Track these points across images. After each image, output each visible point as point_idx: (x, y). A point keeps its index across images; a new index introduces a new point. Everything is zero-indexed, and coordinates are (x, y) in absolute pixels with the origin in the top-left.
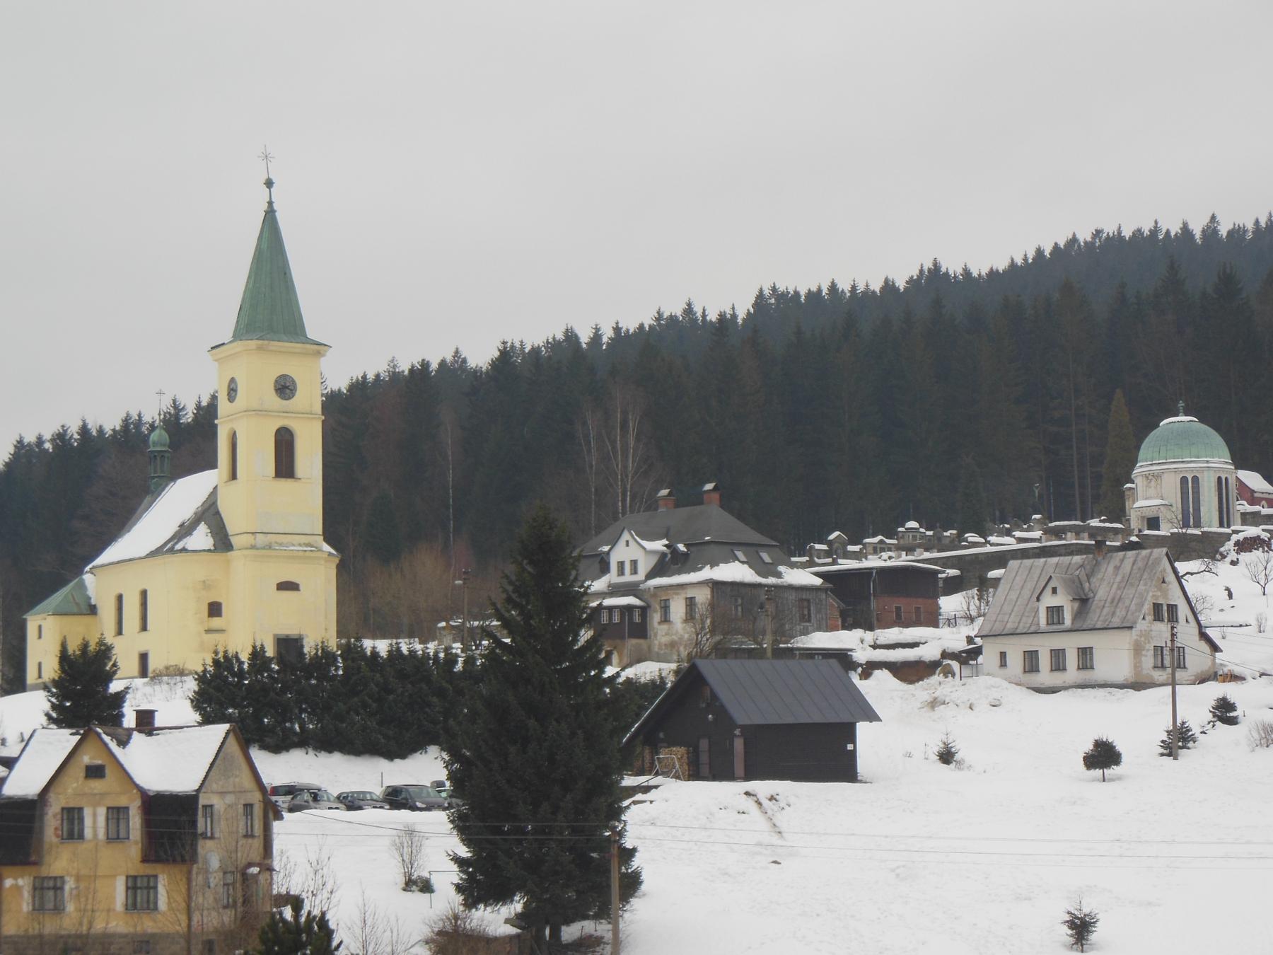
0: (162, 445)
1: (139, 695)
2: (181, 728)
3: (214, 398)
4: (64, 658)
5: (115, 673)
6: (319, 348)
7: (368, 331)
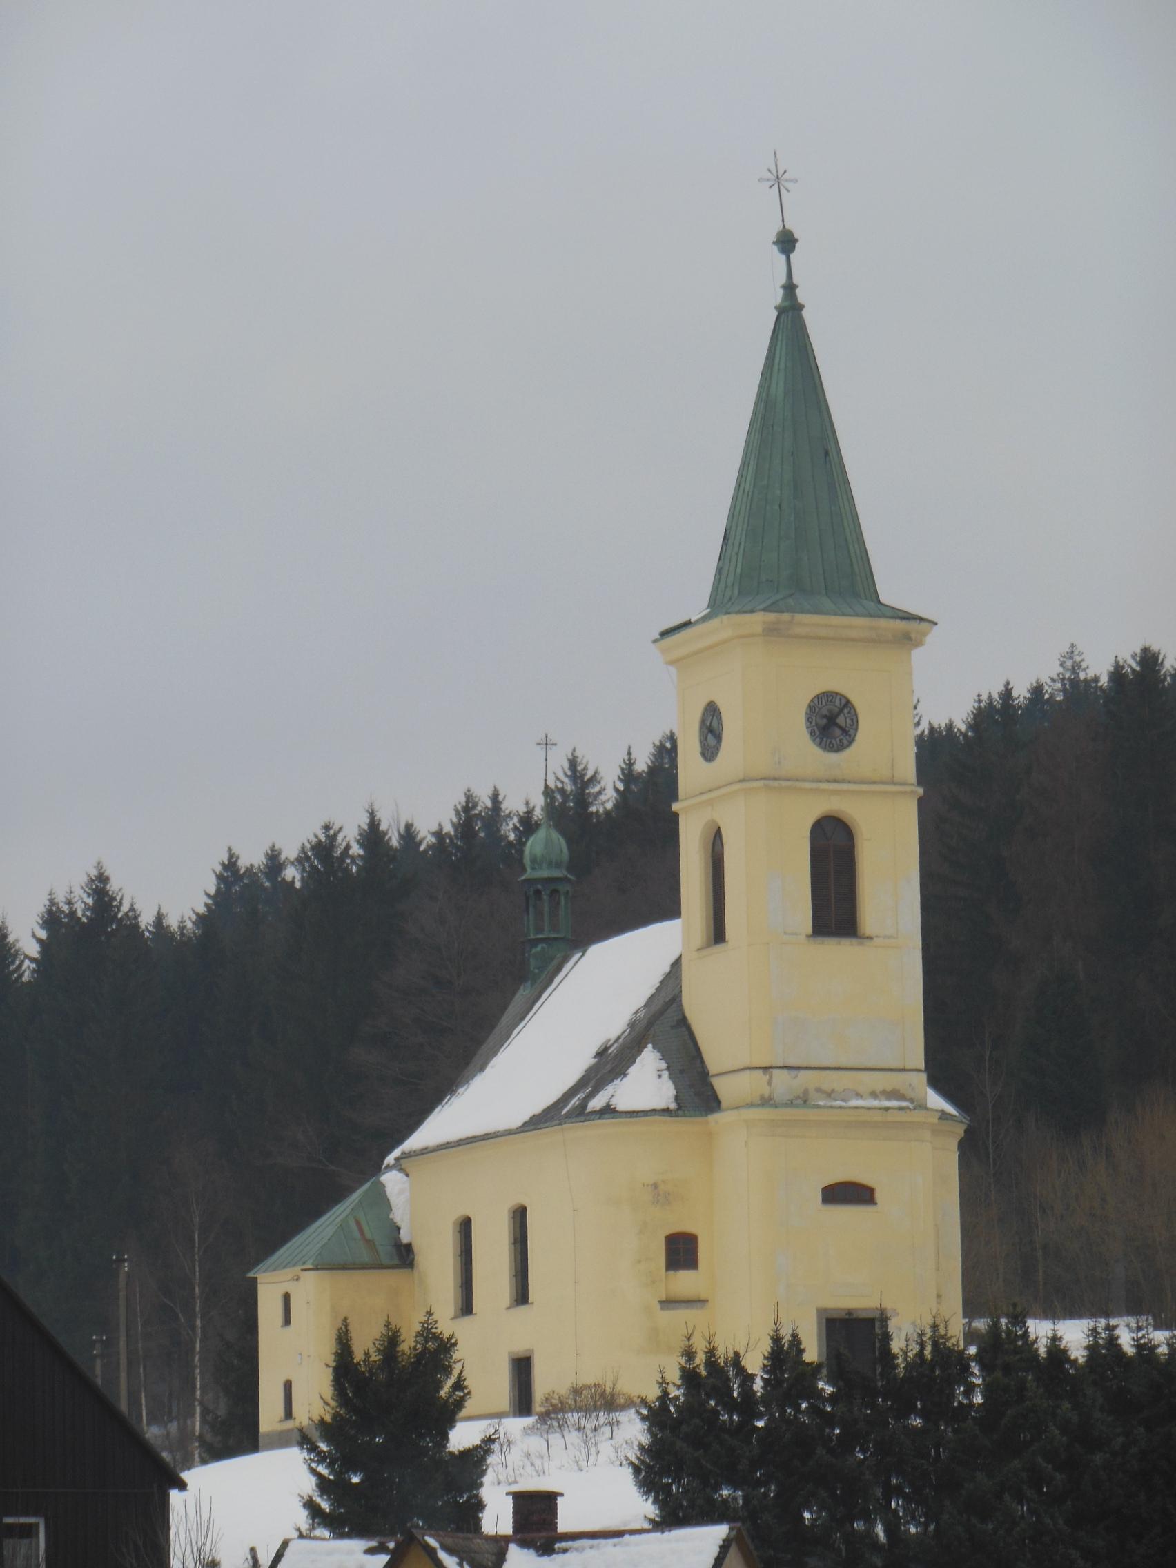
0: (558, 865)
1: (514, 1456)
2: (618, 1534)
3: (667, 752)
4: (345, 1369)
5: (460, 1404)
6: (909, 628)
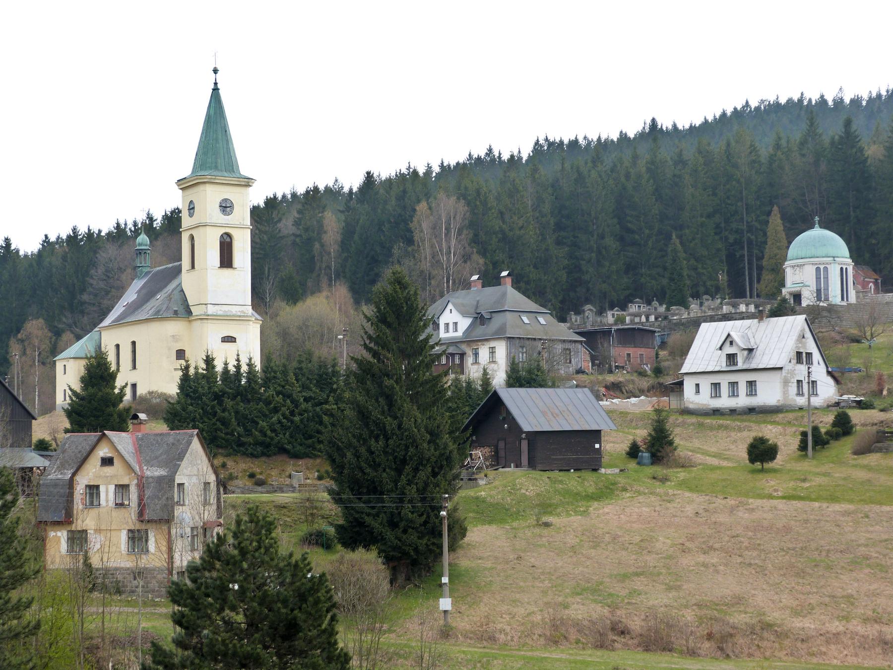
6: (247, 183)
7: (281, 163)
